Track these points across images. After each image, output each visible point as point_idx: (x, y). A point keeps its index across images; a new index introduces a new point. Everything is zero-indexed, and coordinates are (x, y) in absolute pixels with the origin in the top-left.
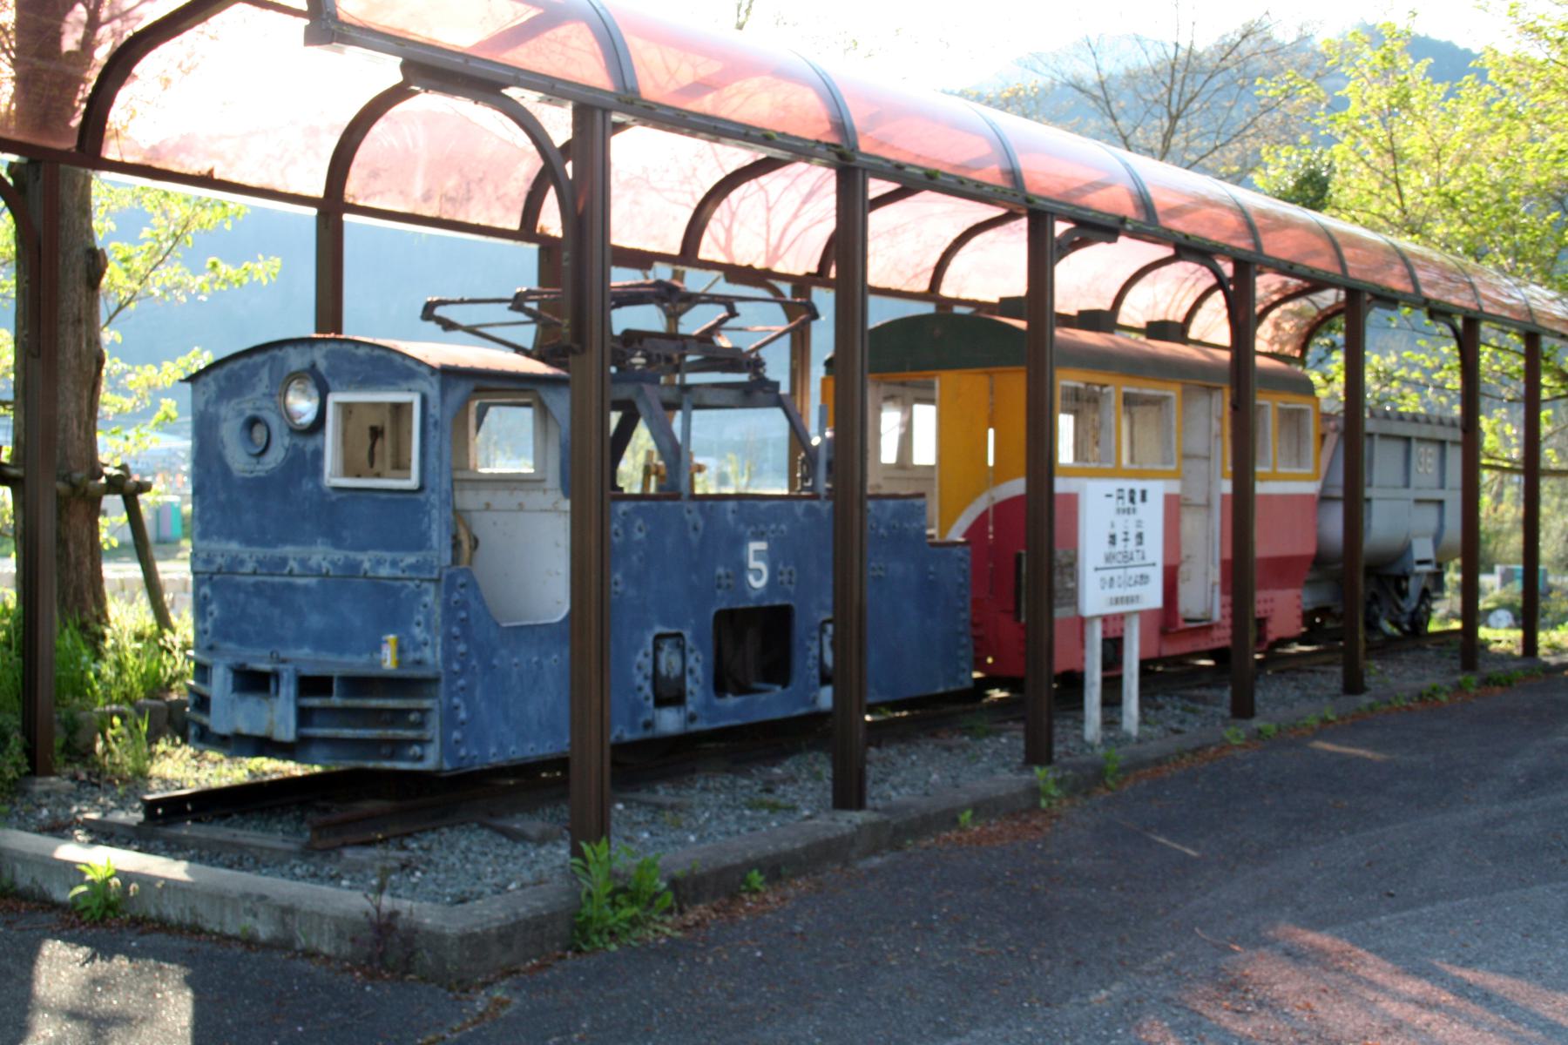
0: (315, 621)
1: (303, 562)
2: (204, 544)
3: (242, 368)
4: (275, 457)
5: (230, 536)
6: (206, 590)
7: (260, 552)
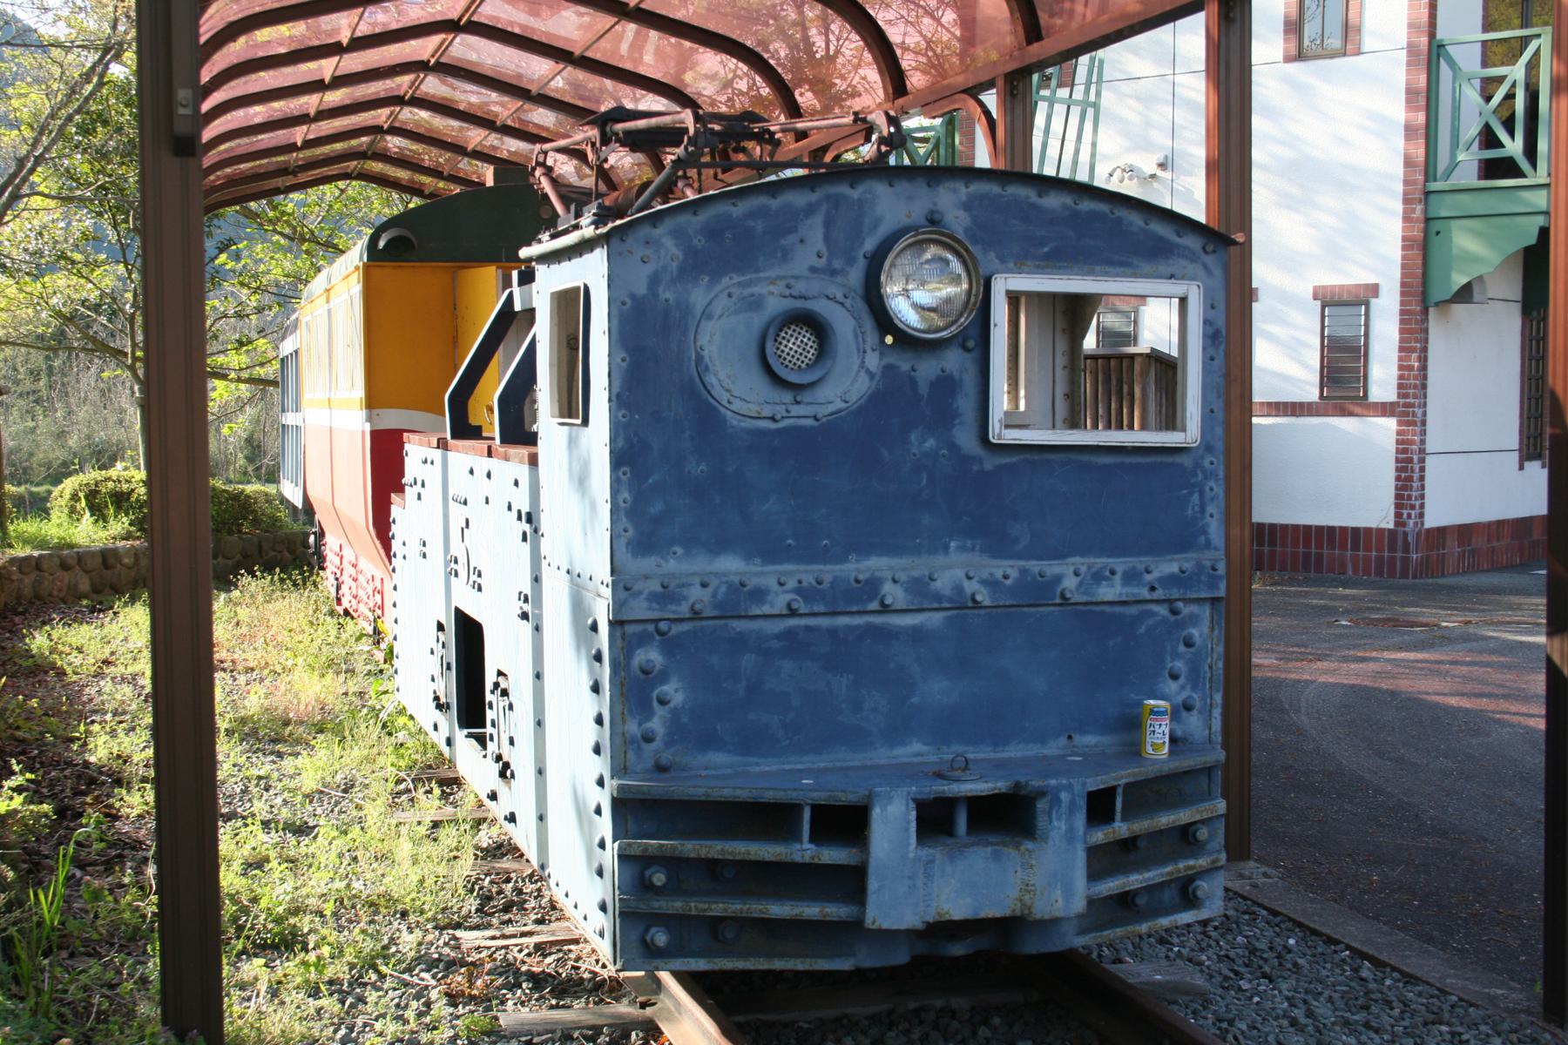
0: (937, 690)
1: (919, 587)
2: (648, 563)
3: (751, 215)
4: (847, 384)
5: (720, 546)
6: (652, 655)
7: (806, 573)
